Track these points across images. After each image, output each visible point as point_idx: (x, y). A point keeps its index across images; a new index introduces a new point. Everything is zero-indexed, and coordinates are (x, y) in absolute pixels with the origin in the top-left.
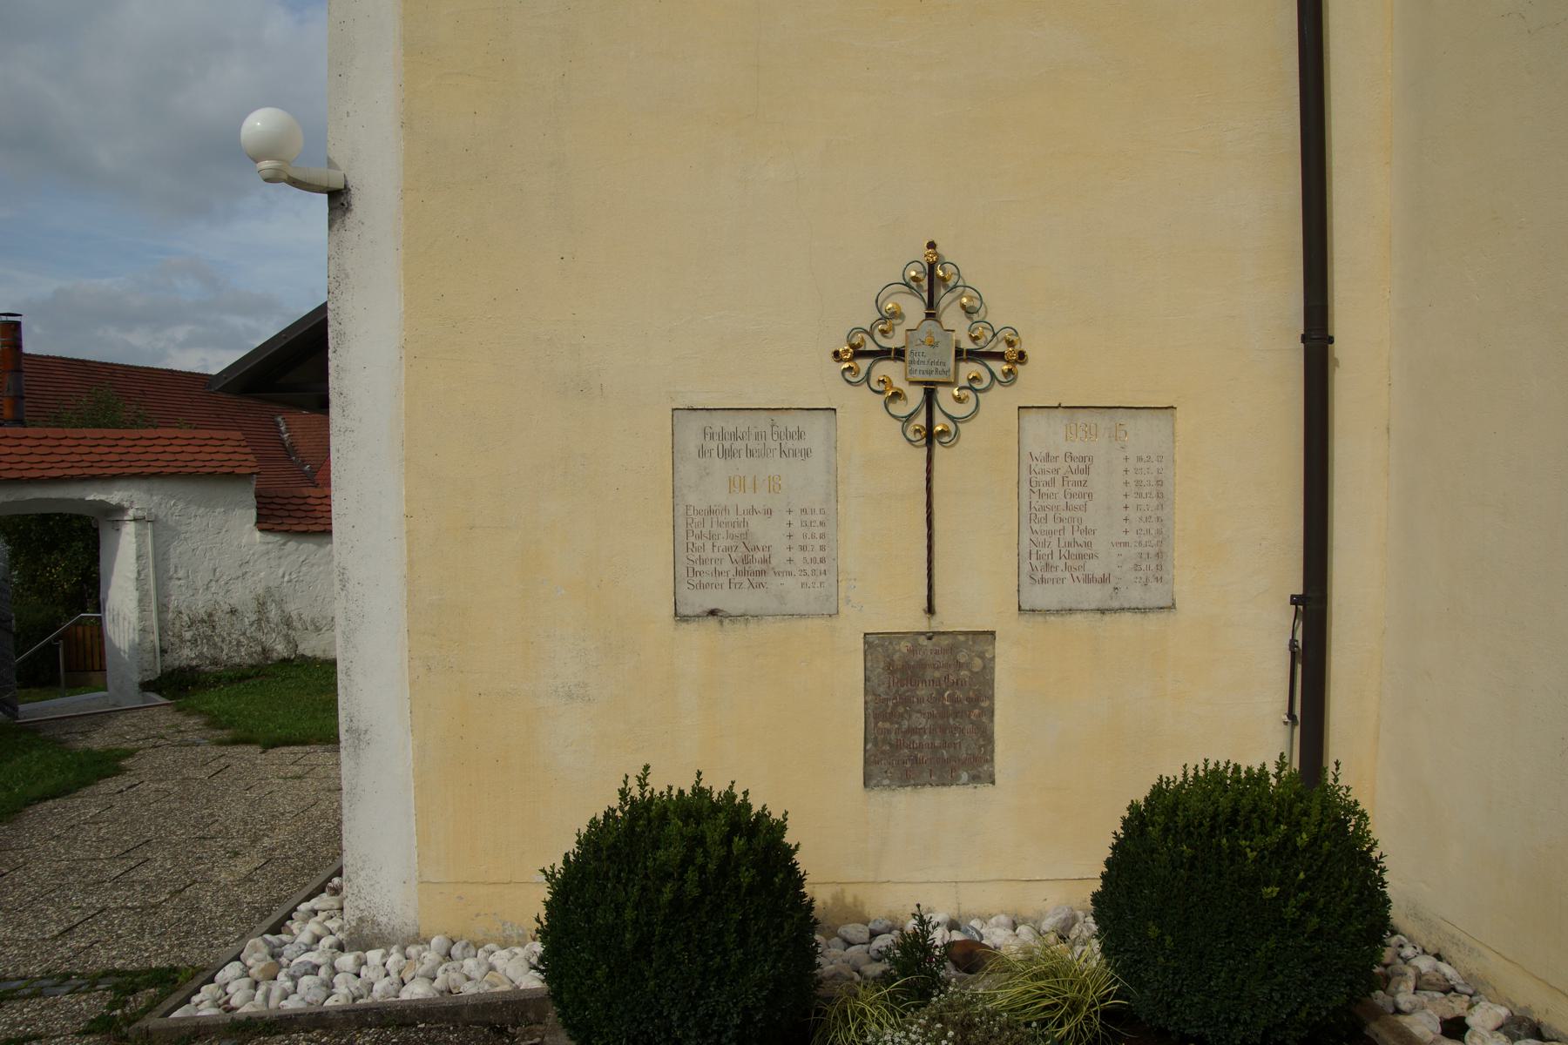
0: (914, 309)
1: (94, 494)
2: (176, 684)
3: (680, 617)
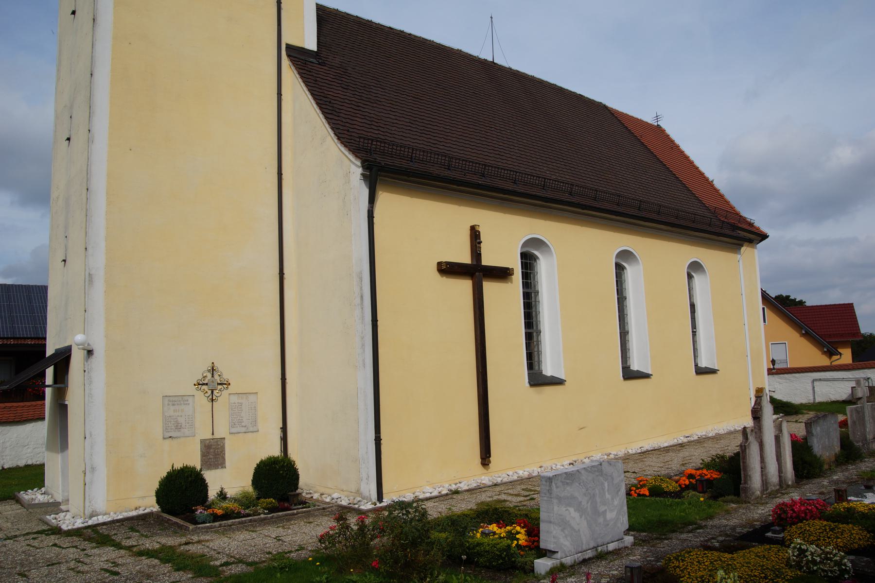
0: (209, 375)
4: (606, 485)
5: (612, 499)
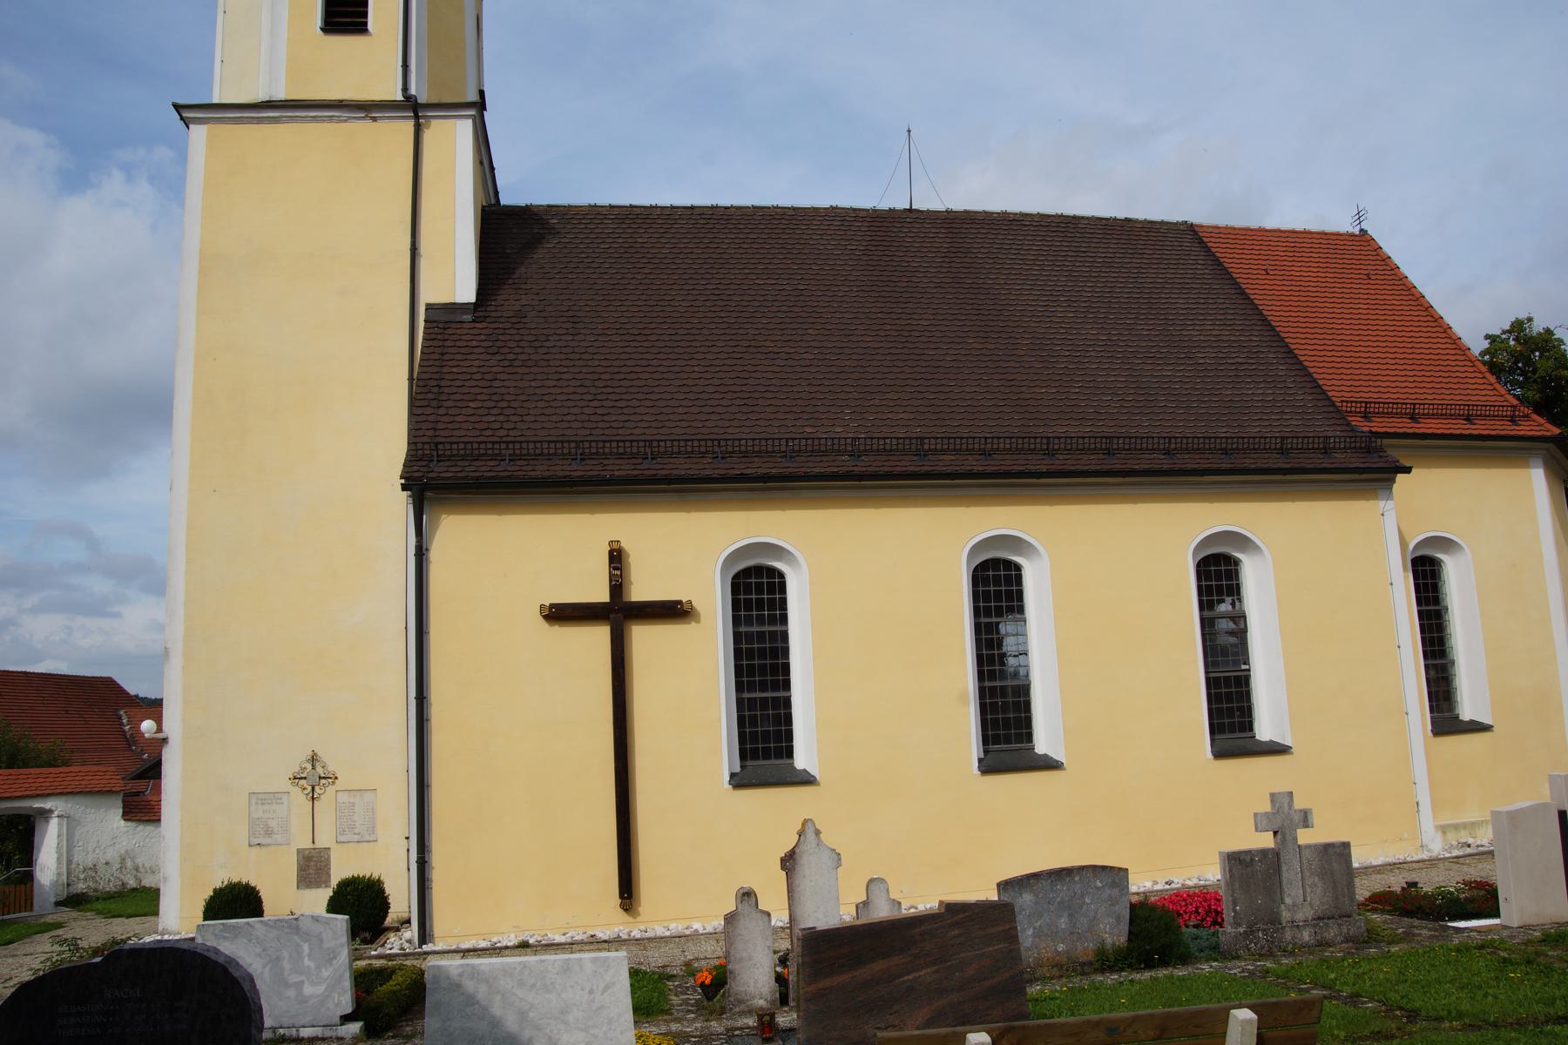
1: (37, 804)
2: (74, 901)
4: (306, 947)
5: (318, 968)
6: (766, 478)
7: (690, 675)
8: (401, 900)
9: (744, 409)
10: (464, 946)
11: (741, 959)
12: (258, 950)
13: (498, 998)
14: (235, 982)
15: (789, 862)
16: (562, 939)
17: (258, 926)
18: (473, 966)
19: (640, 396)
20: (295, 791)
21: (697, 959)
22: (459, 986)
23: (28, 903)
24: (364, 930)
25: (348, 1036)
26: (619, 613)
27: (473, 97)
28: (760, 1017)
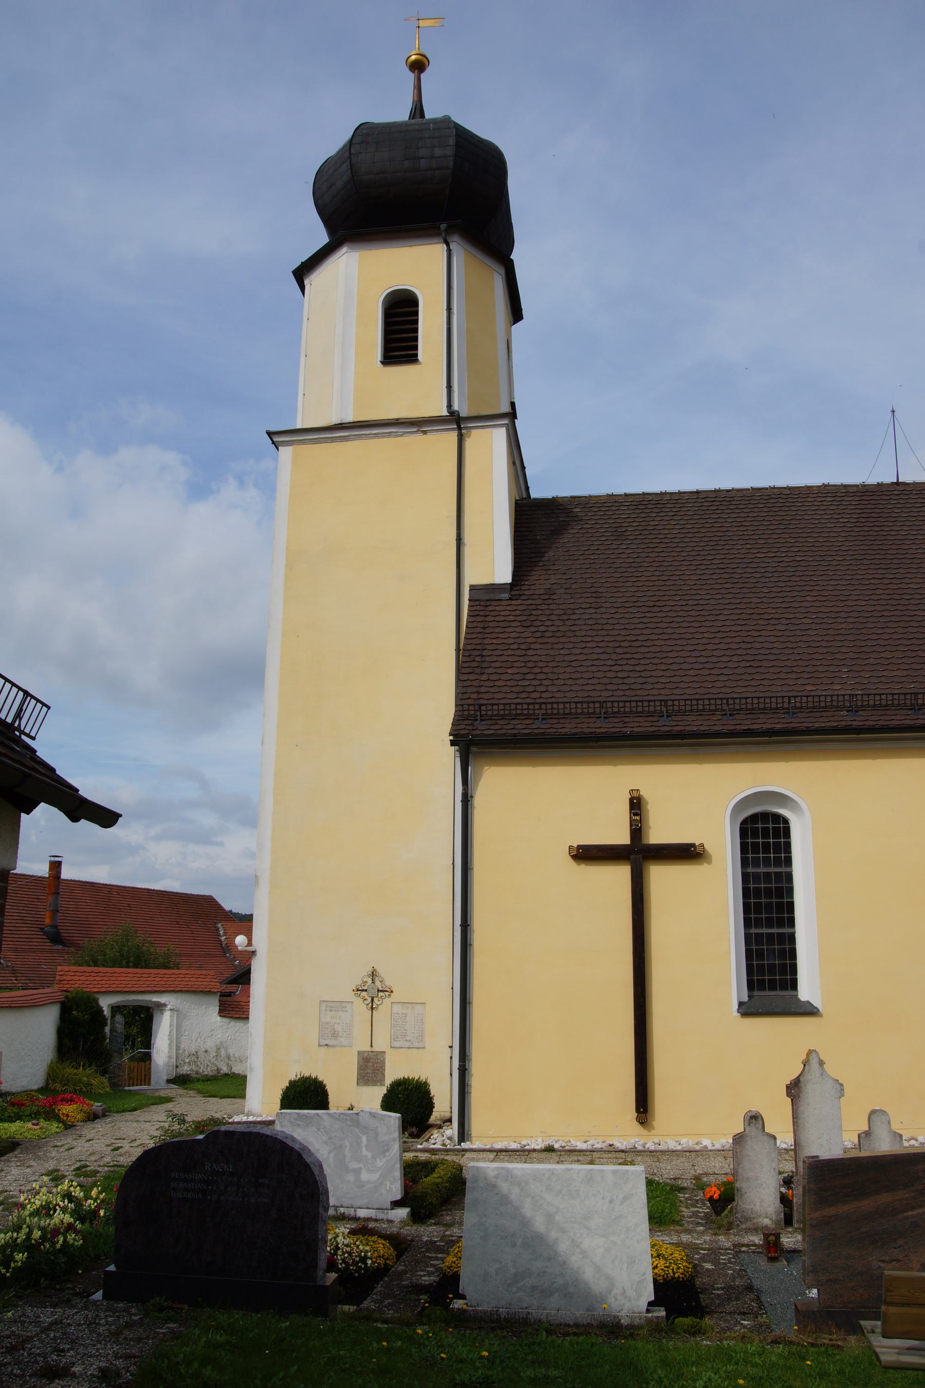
0: (370, 981)
1: (155, 998)
2: (181, 1080)
3: (320, 1046)
4: (364, 1139)
5: (374, 1157)
6: (770, 733)
7: (702, 911)
8: (444, 1101)
9: (750, 670)
10: (499, 1146)
11: (748, 1179)
12: (325, 1138)
13: (528, 1200)
14: (307, 1166)
15: (794, 1089)
16: (584, 1146)
17: (325, 1117)
18: (507, 1170)
19: (656, 661)
20: (358, 1002)
21: (706, 1174)
22: (494, 1186)
23: (146, 1078)
24: (412, 1125)
25: (397, 1220)
26: (639, 854)
27: (506, 409)
28: (766, 1236)
